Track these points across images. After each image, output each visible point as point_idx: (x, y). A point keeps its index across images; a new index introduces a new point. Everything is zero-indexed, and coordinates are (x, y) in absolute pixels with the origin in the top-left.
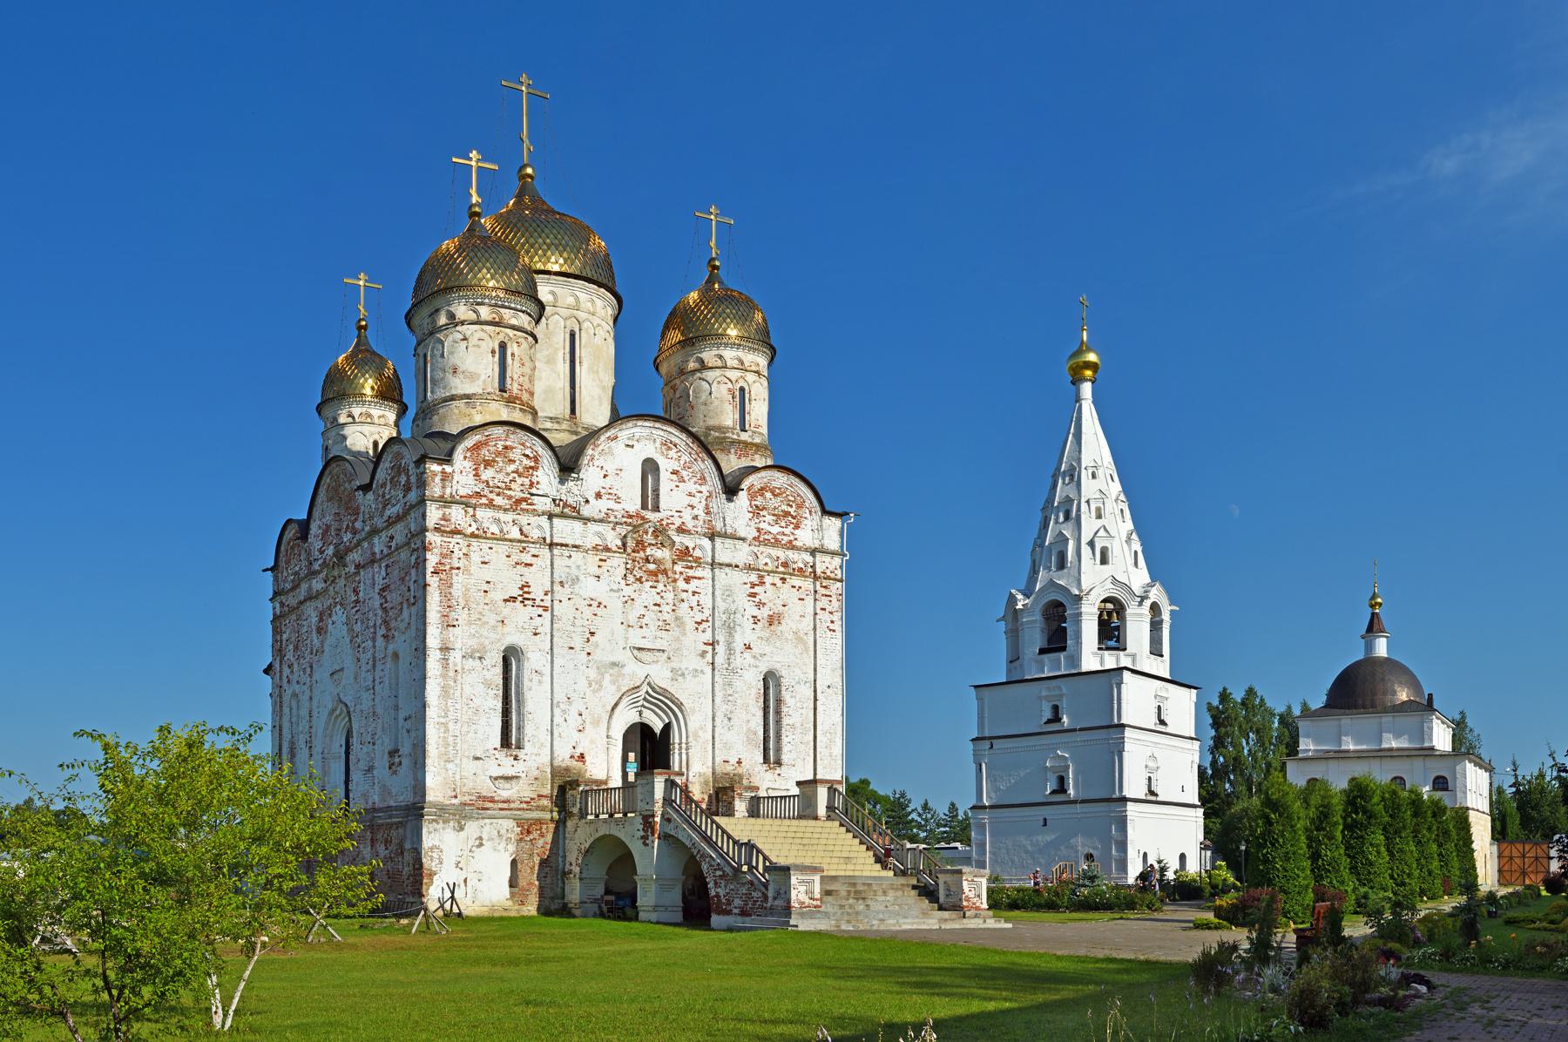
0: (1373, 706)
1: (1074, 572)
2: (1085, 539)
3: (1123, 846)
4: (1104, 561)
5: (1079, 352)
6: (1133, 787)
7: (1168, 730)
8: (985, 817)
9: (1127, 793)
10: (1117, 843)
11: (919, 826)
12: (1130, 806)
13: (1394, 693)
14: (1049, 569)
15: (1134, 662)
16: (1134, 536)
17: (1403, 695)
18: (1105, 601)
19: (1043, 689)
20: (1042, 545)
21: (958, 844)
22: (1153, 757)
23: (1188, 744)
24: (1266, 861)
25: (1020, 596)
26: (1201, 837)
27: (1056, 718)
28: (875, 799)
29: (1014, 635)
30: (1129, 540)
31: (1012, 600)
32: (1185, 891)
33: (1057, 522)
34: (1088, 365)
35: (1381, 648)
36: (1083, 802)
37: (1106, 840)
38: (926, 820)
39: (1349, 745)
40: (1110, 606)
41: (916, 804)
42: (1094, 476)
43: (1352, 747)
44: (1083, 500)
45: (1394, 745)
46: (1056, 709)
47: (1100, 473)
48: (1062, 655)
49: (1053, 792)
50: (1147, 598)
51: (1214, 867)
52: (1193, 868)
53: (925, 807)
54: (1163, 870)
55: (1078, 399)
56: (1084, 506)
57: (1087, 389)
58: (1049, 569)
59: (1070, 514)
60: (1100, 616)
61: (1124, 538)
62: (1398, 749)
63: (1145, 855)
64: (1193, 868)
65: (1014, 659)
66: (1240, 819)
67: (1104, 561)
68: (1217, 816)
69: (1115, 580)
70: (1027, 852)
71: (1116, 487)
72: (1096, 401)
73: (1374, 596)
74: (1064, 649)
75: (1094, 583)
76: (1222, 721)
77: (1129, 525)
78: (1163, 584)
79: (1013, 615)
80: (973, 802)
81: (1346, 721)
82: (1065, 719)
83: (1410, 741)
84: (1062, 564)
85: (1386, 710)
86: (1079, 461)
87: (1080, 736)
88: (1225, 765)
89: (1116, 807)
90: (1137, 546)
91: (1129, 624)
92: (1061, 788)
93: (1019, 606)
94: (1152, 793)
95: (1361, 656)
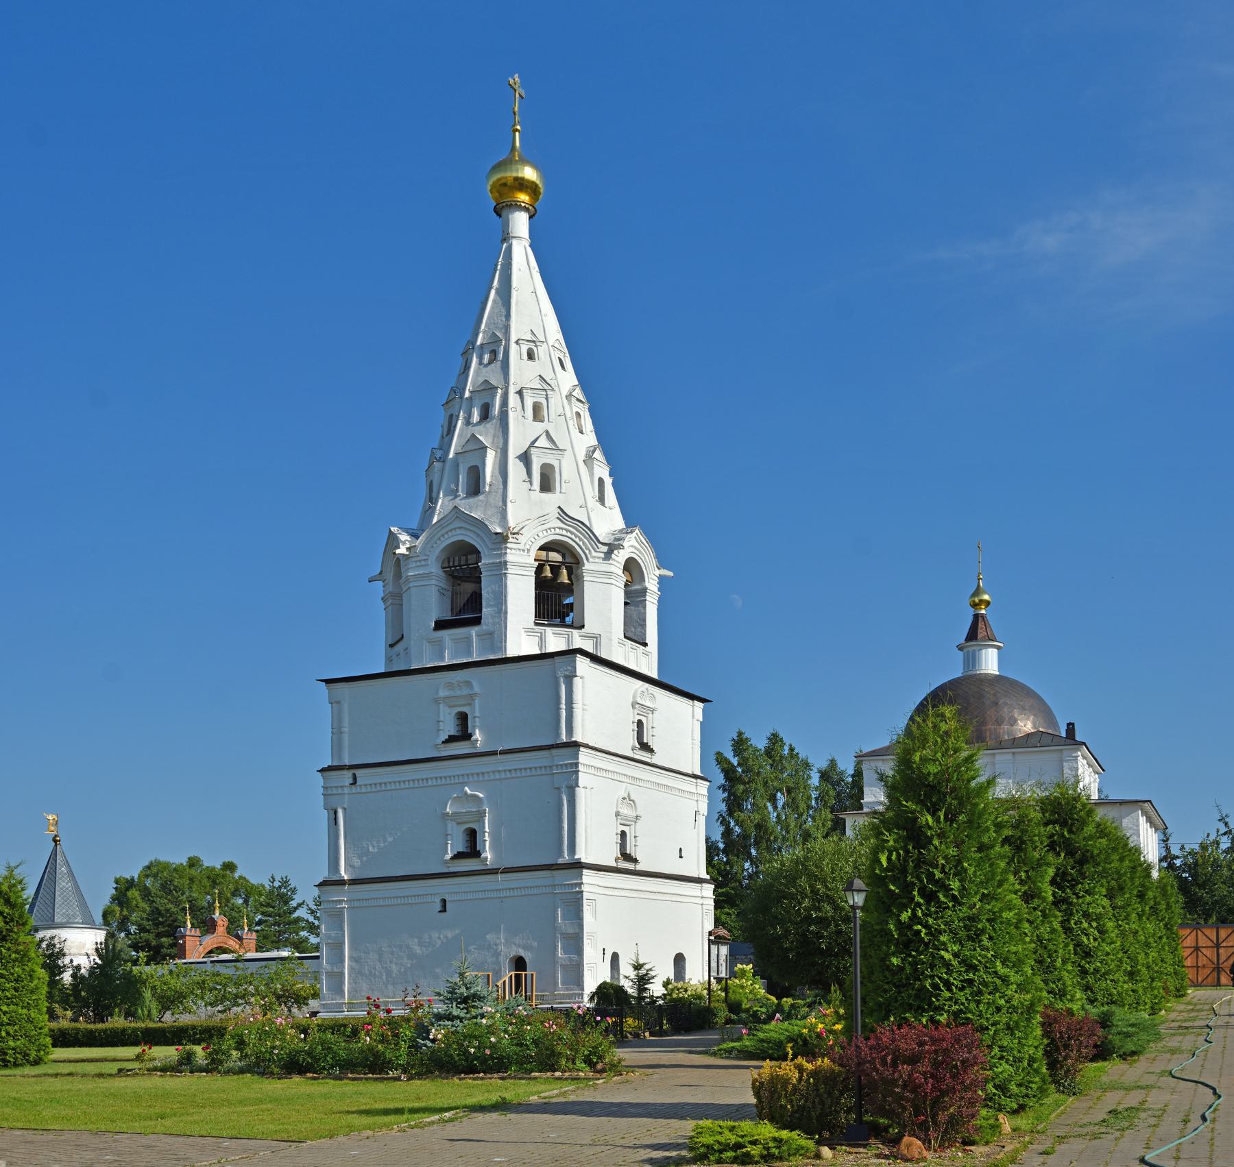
1: (496, 500)
2: (514, 451)
3: (575, 943)
4: (546, 486)
6: (595, 843)
7: (655, 760)
8: (342, 897)
9: (583, 855)
10: (566, 937)
12: (588, 877)
13: (1013, 722)
15: (596, 646)
16: (598, 455)
17: (1026, 726)
18: (545, 548)
20: (443, 459)
22: (629, 800)
23: (688, 785)
24: (910, 942)
25: (404, 537)
26: (710, 925)
27: (464, 735)
28: (245, 889)
29: (395, 602)
30: (589, 460)
31: (393, 541)
32: (682, 1017)
33: (468, 422)
34: (522, 185)
35: (990, 662)
40: (555, 557)
42: (531, 356)
46: (463, 718)
47: (541, 351)
48: (473, 631)
49: (458, 856)
50: (620, 547)
51: (733, 974)
52: (696, 975)
54: (643, 981)
55: (506, 237)
56: (513, 400)
57: (520, 223)
58: (454, 494)
59: (490, 411)
60: (539, 570)
61: (581, 456)
63: (615, 957)
64: (696, 975)
66: (793, 880)
67: (546, 486)
68: (733, 905)
69: (563, 514)
71: (568, 379)
73: (977, 592)
74: (477, 621)
75: (528, 522)
76: (742, 777)
77: (591, 439)
78: (647, 533)
80: (324, 874)
82: (478, 735)
84: (475, 488)
85: (1000, 745)
86: (507, 329)
88: (745, 837)
90: (602, 471)
92: (472, 850)
93: (402, 550)
94: (627, 857)
95: (958, 673)
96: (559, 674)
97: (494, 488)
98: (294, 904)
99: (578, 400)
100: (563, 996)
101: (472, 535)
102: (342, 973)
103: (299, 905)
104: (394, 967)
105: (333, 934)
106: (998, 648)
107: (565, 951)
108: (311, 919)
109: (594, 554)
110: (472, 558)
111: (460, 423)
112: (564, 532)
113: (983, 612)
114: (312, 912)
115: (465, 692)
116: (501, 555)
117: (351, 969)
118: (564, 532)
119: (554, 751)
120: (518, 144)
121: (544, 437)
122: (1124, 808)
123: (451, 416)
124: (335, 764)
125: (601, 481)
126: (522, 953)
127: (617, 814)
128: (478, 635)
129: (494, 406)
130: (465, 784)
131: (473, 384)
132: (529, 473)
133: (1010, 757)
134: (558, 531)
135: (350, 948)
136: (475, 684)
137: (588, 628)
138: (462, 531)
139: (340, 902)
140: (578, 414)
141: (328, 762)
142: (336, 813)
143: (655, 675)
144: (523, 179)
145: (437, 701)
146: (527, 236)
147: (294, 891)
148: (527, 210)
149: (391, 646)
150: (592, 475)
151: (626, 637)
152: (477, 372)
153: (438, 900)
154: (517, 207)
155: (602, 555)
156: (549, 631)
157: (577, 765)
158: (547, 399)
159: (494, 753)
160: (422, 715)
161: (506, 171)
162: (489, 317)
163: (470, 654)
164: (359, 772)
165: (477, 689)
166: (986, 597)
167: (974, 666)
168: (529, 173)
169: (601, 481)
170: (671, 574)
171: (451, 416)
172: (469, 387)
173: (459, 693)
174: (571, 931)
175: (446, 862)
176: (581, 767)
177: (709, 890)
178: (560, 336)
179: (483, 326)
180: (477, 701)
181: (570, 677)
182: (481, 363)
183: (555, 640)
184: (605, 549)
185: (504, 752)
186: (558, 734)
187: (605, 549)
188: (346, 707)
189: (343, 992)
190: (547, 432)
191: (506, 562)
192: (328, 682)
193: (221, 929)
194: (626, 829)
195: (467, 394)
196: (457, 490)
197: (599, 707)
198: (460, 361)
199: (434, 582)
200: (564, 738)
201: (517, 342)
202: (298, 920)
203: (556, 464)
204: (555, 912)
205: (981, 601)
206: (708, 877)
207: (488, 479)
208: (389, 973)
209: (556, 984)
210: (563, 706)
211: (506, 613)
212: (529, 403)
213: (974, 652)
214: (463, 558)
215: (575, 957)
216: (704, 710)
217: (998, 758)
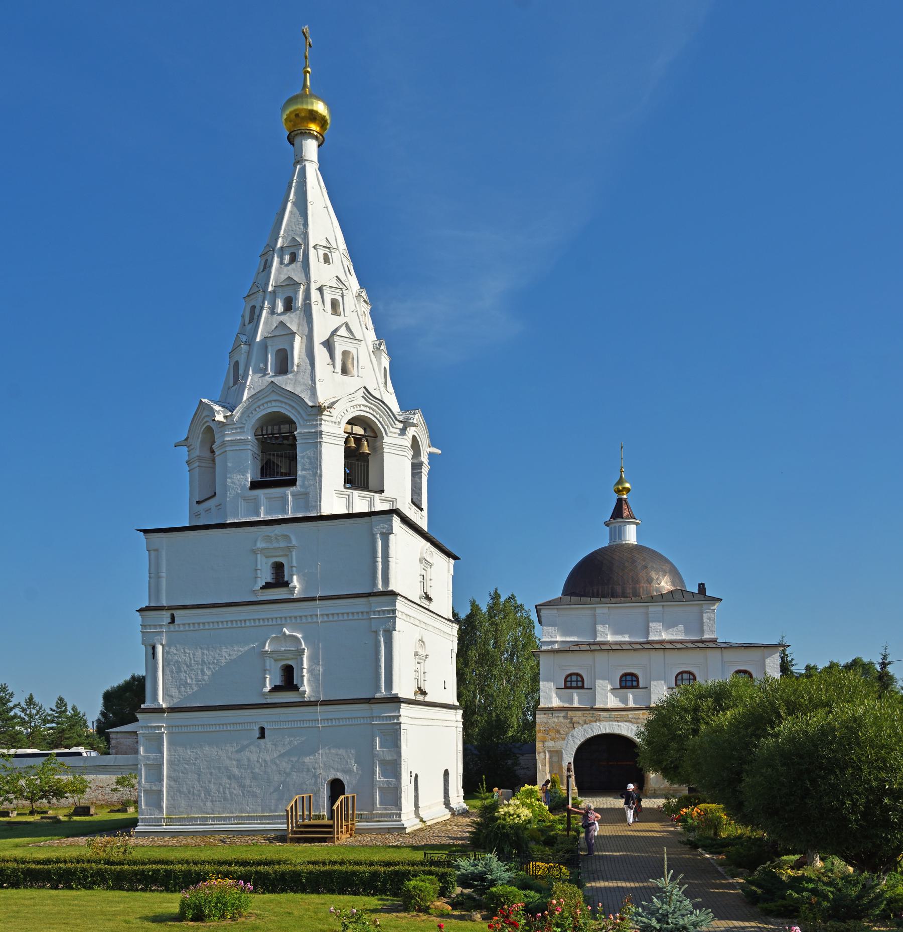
0: (636, 594)
4: (345, 371)
5: (301, 97)
6: (403, 687)
10: (383, 763)
11: (23, 723)
14: (264, 372)
17: (665, 585)
19: (259, 537)
20: (250, 343)
21: (80, 749)
27: (279, 580)
33: (272, 311)
34: (313, 116)
35: (631, 535)
36: (325, 703)
37: (367, 760)
38: (31, 716)
39: (660, 633)
40: (359, 430)
41: (20, 698)
42: (327, 260)
43: (610, 638)
44: (314, 287)
45: (665, 636)
46: (278, 568)
48: (289, 492)
49: (276, 689)
53: (30, 701)
55: (299, 159)
56: (315, 295)
57: (311, 148)
62: (671, 642)
65: (207, 494)
70: (231, 777)
71: (353, 282)
72: (323, 169)
73: (621, 481)
74: (293, 483)
79: (210, 433)
81: (602, 609)
82: (295, 582)
83: (687, 632)
84: (283, 365)
85: (652, 599)
86: (305, 235)
87: (319, 608)
89: (386, 711)
91: (387, 458)
92: (289, 680)
95: (605, 543)
96: (376, 530)
97: (302, 368)
98: (11, 705)
99: (365, 301)
100: (382, 815)
101: (287, 407)
102: (161, 791)
103: (15, 706)
104: (212, 786)
105: (152, 756)
106: (637, 524)
107: (383, 774)
108: (23, 715)
109: (392, 429)
110: (285, 428)
111: (264, 313)
112: (368, 410)
113: (625, 496)
114: (23, 710)
115: (283, 544)
116: (316, 426)
117: (169, 787)
118: (368, 410)
119: (372, 599)
120: (308, 83)
121: (344, 327)
122: (766, 651)
123: (254, 307)
124: (152, 604)
125: (385, 368)
126: (340, 776)
127: (416, 654)
128: (293, 495)
129: (297, 299)
130: (283, 626)
131: (276, 280)
132: (332, 357)
133: (661, 608)
134: (362, 408)
135: (168, 768)
136: (293, 538)
137: (387, 493)
138: (277, 404)
139: (160, 727)
141: (145, 604)
142: (154, 648)
144: (317, 112)
145: (254, 552)
146: (316, 160)
147: (11, 695)
148: (316, 138)
149: (198, 502)
150: (380, 363)
151: (413, 502)
152: (279, 271)
153: (256, 728)
154: (309, 134)
155: (398, 431)
156: (356, 493)
157: (394, 611)
158: (342, 297)
159: (313, 599)
160: (238, 565)
161: (302, 103)
162: (287, 225)
163: (285, 511)
164: (177, 613)
165: (294, 542)
166: (627, 485)
167: (620, 538)
168: (320, 107)
169: (385, 368)
170: (440, 452)
171: (254, 307)
172: (272, 281)
173: (275, 545)
174: (389, 758)
175: (264, 694)
176: (397, 614)
177: (461, 712)
178: (345, 247)
179: (282, 232)
180: (294, 553)
181: (386, 536)
182: (281, 263)
184: (401, 426)
185: (322, 598)
186: (375, 584)
187: (401, 426)
188: (164, 554)
189: (162, 808)
190: (347, 325)
191: (321, 432)
192: (146, 531)
195: (270, 289)
196: (266, 369)
198: (259, 263)
199: (249, 447)
200: (380, 587)
201: (314, 247)
202: (15, 716)
203: (354, 351)
204: (373, 741)
205: (624, 488)
206: (458, 704)
207: (296, 361)
208: (208, 792)
209: (373, 804)
210: (379, 559)
211: (321, 476)
212: (328, 298)
213: (620, 527)
214: (270, 428)
215: (393, 781)
216: (454, 566)
217: (651, 609)
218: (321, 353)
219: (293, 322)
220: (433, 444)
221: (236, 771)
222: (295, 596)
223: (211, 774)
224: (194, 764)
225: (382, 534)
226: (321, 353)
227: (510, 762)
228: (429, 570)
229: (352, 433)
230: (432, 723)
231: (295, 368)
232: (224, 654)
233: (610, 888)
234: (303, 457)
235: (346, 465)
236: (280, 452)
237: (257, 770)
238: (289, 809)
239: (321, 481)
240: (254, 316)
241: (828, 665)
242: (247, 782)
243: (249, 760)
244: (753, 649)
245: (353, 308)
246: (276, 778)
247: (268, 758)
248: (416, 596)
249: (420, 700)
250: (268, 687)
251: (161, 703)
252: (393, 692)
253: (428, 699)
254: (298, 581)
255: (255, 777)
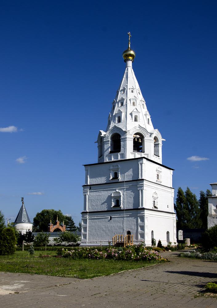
4: (136, 120)
6: (147, 203)
9: (144, 206)
22: (156, 193)
27: (116, 177)
34: (131, 55)
40: (138, 136)
42: (132, 92)
44: (128, 99)
49: (113, 179)
52: (173, 241)
57: (130, 63)
60: (134, 139)
65: (101, 155)
69: (140, 127)
75: (131, 128)
82: (120, 178)
84: (119, 121)
86: (127, 86)
90: (149, 117)
102: (86, 235)
112: (140, 130)
117: (89, 233)
118: (140, 130)
120: (130, 47)
121: (135, 109)
125: (148, 119)
138: (117, 131)
139: (87, 217)
140: (143, 104)
143: (161, 163)
146: (131, 66)
148: (131, 60)
154: (129, 60)
155: (149, 136)
164: (91, 186)
168: (132, 52)
170: (165, 140)
177: (175, 216)
179: (121, 86)
183: (138, 155)
184: (150, 134)
187: (150, 134)
188: (89, 171)
193: (58, 224)
194: (155, 200)
195: (114, 115)
197: (148, 171)
203: (138, 115)
211: (126, 149)
218: (129, 116)
219: (122, 109)
220: (163, 138)
221: (104, 229)
222: (120, 181)
223: (98, 229)
224: (95, 227)
225: (141, 164)
226: (129, 116)
227: (88, 249)
228: (160, 173)
229: (136, 137)
230: (169, 218)
231: (122, 121)
232: (102, 197)
233: (121, 85)
234: (122, 144)
235: (134, 143)
236: (117, 140)
237: (109, 229)
238: (113, 238)
239: (126, 150)
240: (109, 124)
241: (200, 195)
242: (107, 232)
243: (107, 226)
244: (214, 198)
245: (139, 104)
246: (114, 230)
247: (112, 225)
248: (151, 207)
249: (155, 209)
250: (111, 178)
251: (87, 210)
252: (143, 207)
253: (158, 210)
254: (120, 177)
255: (109, 231)
